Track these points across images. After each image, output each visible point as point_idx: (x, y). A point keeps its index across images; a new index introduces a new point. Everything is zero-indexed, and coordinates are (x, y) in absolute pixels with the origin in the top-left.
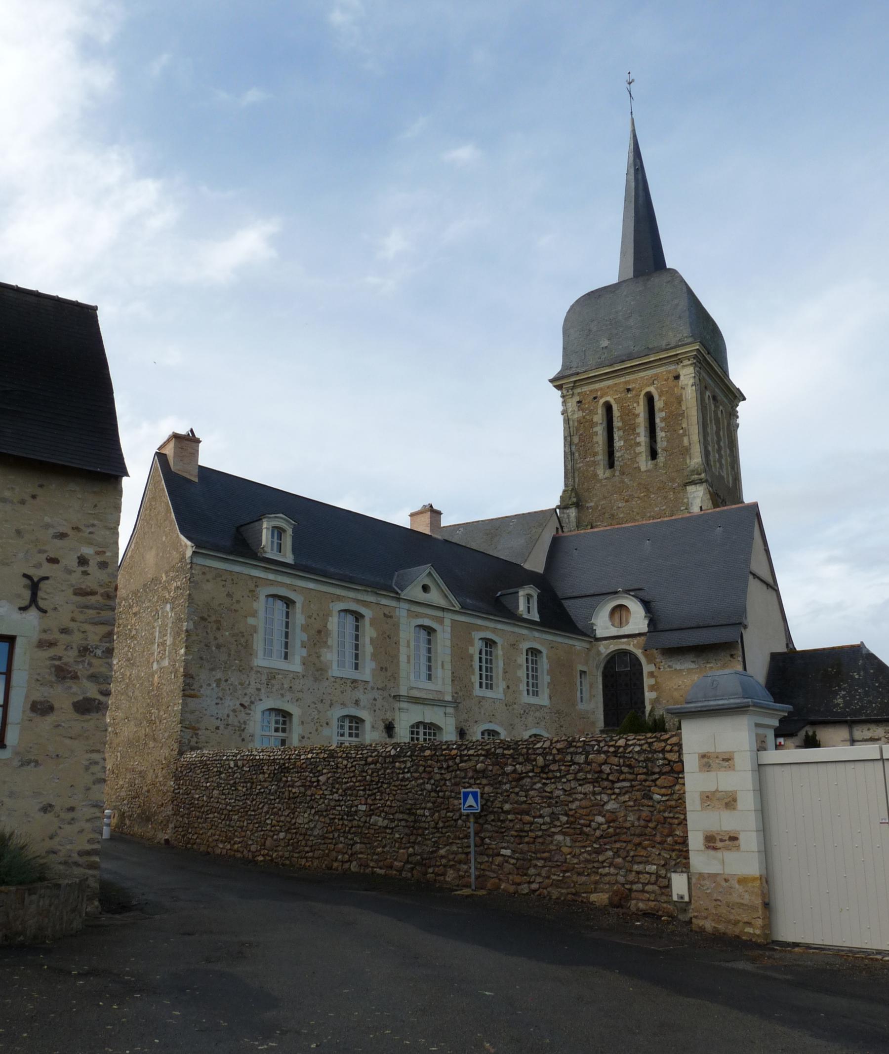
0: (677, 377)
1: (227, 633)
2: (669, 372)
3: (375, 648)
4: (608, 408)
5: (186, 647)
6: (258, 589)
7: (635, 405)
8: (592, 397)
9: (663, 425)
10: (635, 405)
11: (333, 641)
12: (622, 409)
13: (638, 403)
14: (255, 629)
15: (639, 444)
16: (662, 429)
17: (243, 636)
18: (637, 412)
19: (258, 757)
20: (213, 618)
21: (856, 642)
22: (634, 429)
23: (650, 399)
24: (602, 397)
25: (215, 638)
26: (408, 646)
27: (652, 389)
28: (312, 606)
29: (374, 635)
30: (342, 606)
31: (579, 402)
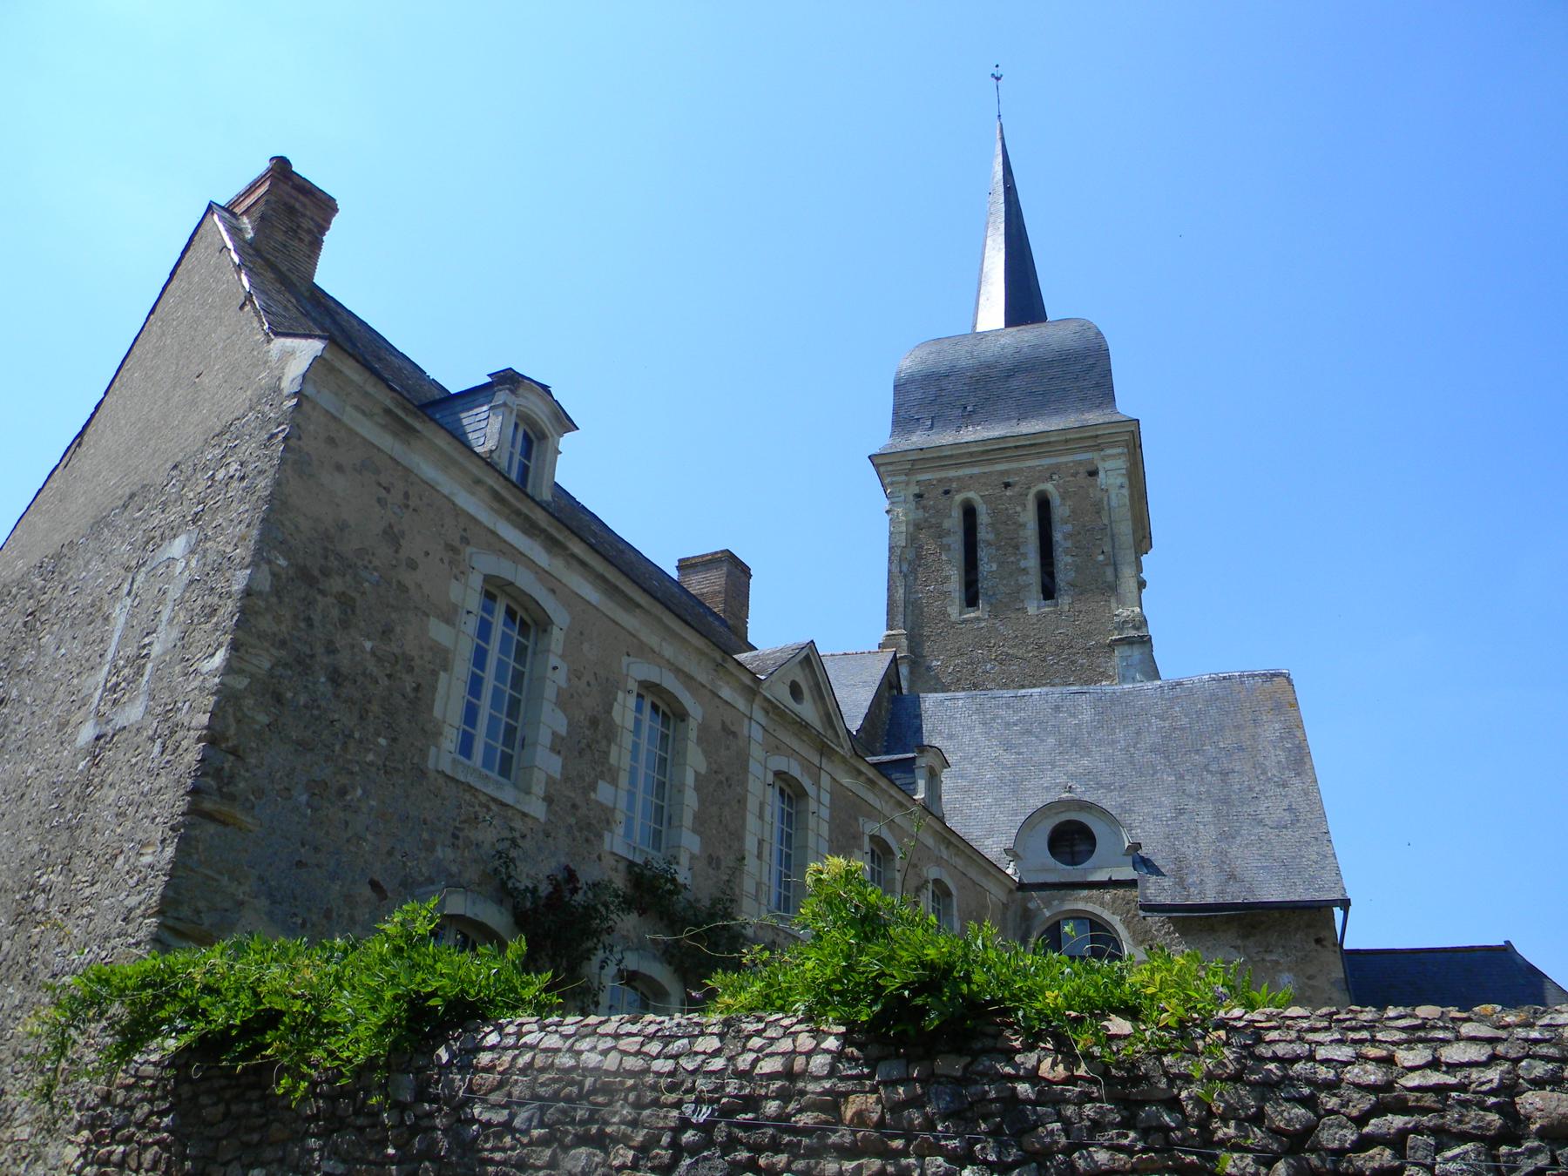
0: (1093, 473)
1: (368, 645)
2: (1080, 463)
3: (702, 802)
4: (969, 512)
5: (235, 646)
6: (469, 550)
7: (1019, 509)
8: (941, 490)
9: (1069, 544)
10: (1019, 509)
11: (619, 756)
12: (994, 513)
13: (1024, 506)
14: (443, 659)
15: (1025, 571)
16: (1067, 552)
17: (410, 670)
18: (1021, 520)
19: (567, 1061)
20: (336, 584)
21: (1498, 941)
22: (1017, 547)
23: (1044, 504)
24: (958, 491)
25: (331, 650)
26: (761, 817)
27: (1049, 487)
28: (586, 646)
29: (703, 770)
30: (652, 674)
31: (919, 496)
